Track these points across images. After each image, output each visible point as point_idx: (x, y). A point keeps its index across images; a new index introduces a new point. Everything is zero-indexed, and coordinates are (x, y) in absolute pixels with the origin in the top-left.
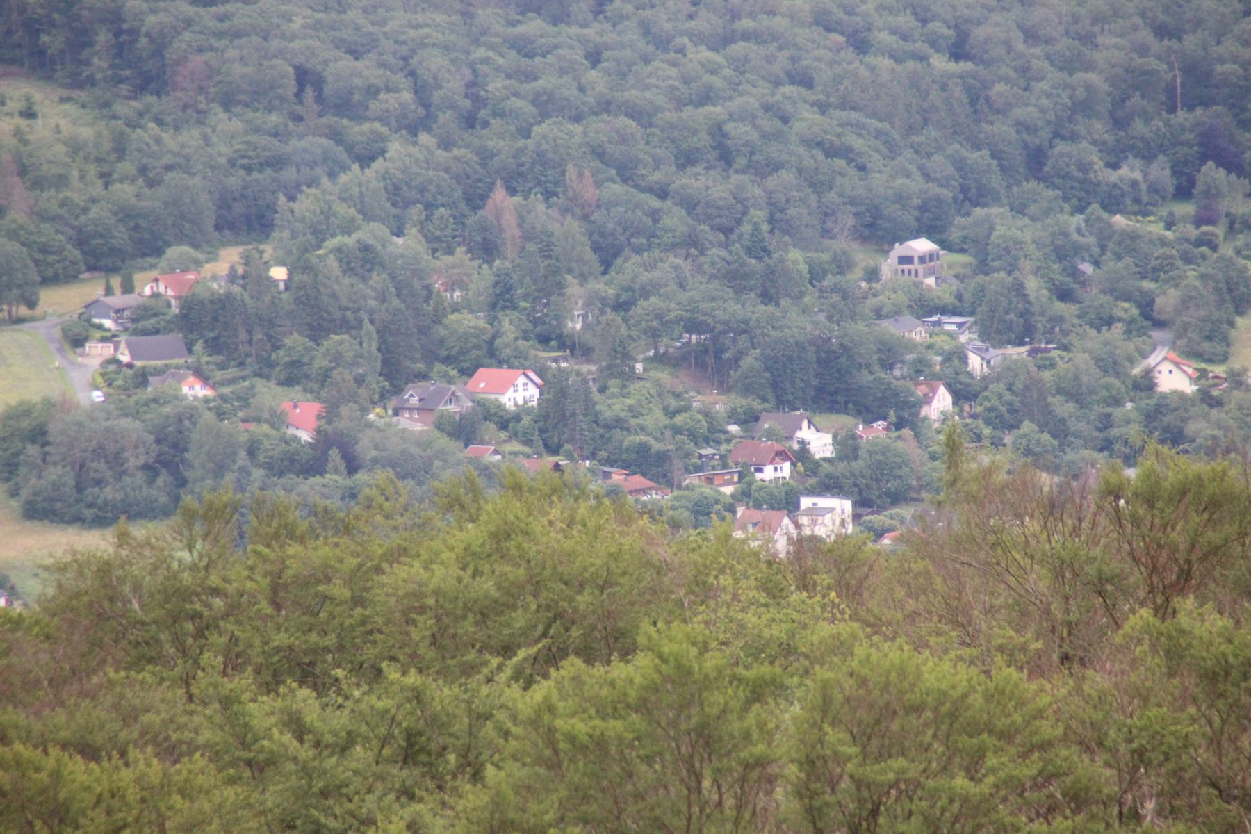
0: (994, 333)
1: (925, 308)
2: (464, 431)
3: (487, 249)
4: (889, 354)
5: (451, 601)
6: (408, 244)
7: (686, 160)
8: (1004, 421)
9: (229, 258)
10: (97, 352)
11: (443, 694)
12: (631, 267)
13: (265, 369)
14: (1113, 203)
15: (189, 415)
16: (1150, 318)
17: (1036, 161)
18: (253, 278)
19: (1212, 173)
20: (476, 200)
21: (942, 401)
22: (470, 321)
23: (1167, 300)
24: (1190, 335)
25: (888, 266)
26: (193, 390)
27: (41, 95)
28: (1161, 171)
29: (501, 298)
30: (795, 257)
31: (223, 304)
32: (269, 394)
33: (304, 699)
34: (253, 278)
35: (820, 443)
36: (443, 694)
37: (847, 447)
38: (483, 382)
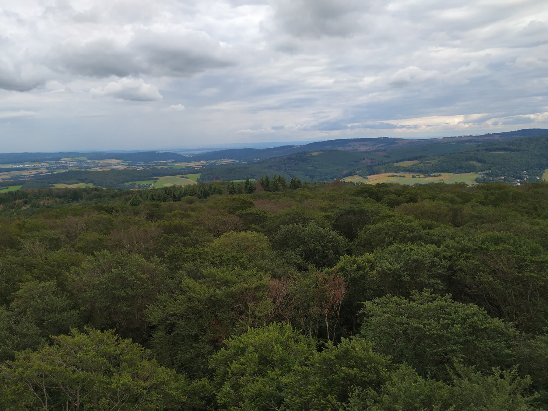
0: (529, 176)
1: (525, 174)
2: (500, 179)
3: (502, 171)
4: (523, 177)
5: (118, 268)
6: (497, 170)
7: (513, 167)
8: (529, 180)
9: (488, 171)
10: (481, 175)
11: (494, 191)
12: (509, 172)
13: (490, 176)
14: (536, 170)
15: (485, 178)
16: (537, 175)
17: (532, 167)
18: (489, 172)
19: (541, 169)
20: (501, 168)
21: (526, 179)
22: (501, 174)
23: (538, 175)
24: (121, 261)
25: (523, 172)
26: (486, 177)
27: (479, 163)
28: (539, 168)
29: (502, 173)
30: (518, 172)
31: (487, 173)
32: (490, 177)
33: (487, 191)
34: (489, 172)
35: (519, 181)
36: (494, 191)
37: (520, 181)
38: (501, 177)
